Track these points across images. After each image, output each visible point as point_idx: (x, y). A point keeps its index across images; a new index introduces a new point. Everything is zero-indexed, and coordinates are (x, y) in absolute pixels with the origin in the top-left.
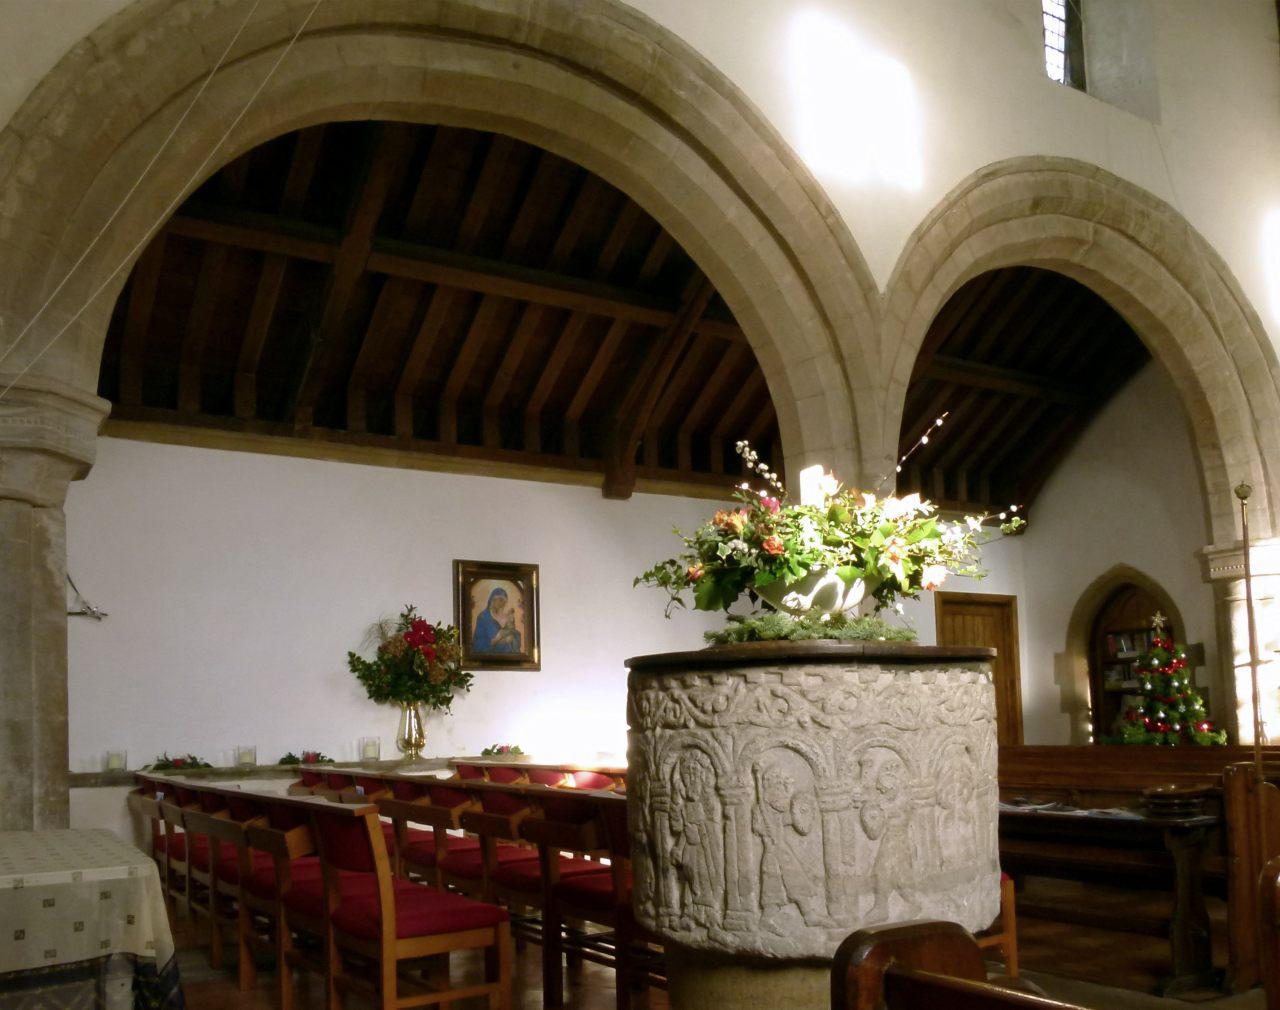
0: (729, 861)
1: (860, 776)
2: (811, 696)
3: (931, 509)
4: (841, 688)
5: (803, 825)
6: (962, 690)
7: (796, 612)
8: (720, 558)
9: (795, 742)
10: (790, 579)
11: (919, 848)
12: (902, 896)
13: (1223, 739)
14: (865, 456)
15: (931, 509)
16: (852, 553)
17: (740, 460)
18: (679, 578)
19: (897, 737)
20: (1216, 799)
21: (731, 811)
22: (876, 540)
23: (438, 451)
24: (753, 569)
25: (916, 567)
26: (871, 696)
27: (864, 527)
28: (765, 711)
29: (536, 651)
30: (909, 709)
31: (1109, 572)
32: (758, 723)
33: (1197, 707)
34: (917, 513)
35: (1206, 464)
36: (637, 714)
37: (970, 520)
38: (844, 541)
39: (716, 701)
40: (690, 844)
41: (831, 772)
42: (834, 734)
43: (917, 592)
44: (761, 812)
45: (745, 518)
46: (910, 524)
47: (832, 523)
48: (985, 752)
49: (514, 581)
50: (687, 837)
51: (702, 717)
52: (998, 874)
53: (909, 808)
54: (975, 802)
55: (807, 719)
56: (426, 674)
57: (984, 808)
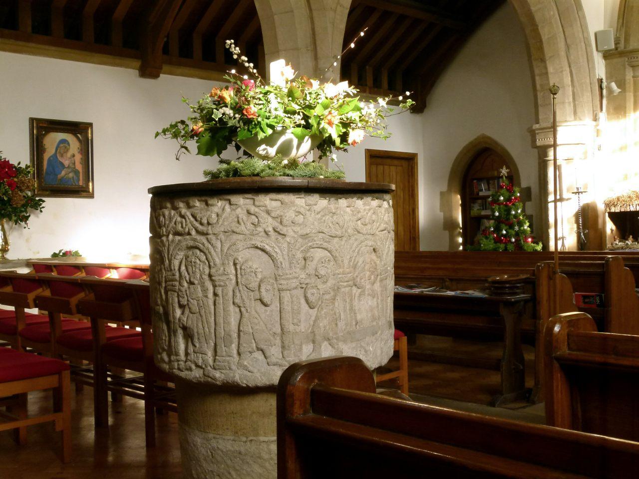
1: (305, 267)
2: (273, 215)
3: (355, 91)
4: (293, 208)
5: (266, 300)
6: (372, 211)
7: (266, 157)
8: (215, 120)
10: (261, 135)
11: (342, 314)
12: (330, 344)
13: (539, 247)
14: (320, 54)
15: (355, 91)
16: (302, 119)
17: (229, 54)
18: (186, 133)
19: (329, 242)
20: (531, 284)
21: (219, 291)
22: (318, 111)
23: (17, 38)
24: (237, 128)
25: (344, 130)
26: (313, 214)
27: (311, 102)
28: (242, 224)
29: (91, 184)
31: (475, 139)
32: (238, 231)
33: (526, 228)
34: (346, 94)
35: (537, 71)
36: (156, 227)
37: (380, 100)
38: (298, 111)
39: (210, 216)
40: (192, 313)
41: (286, 265)
42: (288, 239)
43: (346, 147)
44: (239, 291)
45: (232, 93)
46: (341, 101)
47: (290, 99)
48: (386, 251)
49: (75, 134)
50: (190, 308)
51: (200, 228)
52: (393, 330)
54: (378, 284)
55: (271, 229)
56: (10, 200)
57: (384, 288)
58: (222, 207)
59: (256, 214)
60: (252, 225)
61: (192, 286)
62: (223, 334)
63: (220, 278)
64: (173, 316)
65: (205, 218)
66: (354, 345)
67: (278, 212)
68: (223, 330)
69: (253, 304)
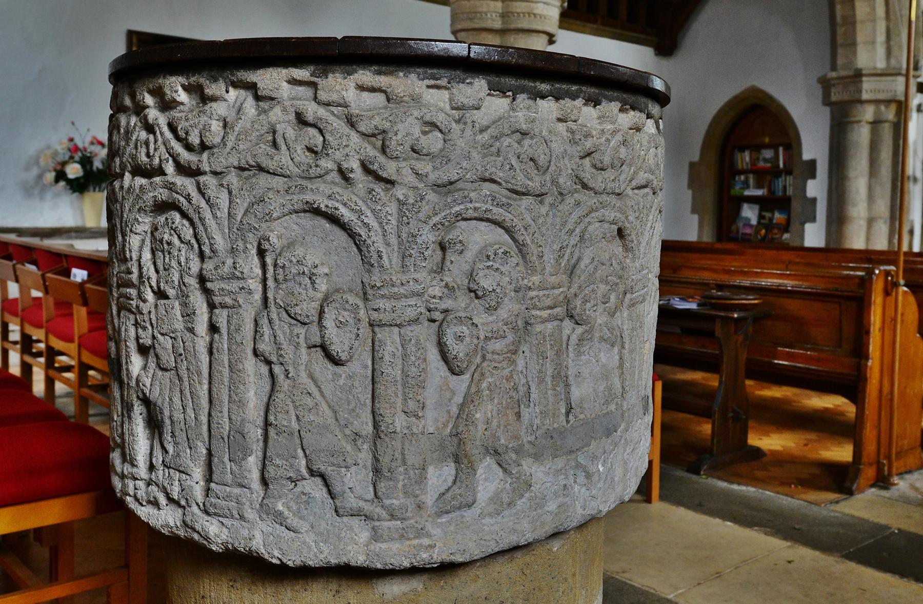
0: (215, 402)
1: (441, 268)
5: (338, 348)
6: (619, 137)
9: (331, 203)
11: (533, 389)
19: (509, 205)
21: (222, 318)
26: (468, 132)
28: (283, 147)
30: (531, 159)
31: (742, 93)
39: (206, 128)
41: (390, 259)
42: (399, 192)
50: (157, 356)
51: (185, 156)
53: (520, 323)
55: (355, 165)
58: (238, 104)
59: (319, 125)
60: (307, 154)
61: (162, 302)
62: (227, 428)
63: (222, 285)
64: (127, 369)
65: (197, 132)
66: (560, 463)
67: (377, 121)
68: (227, 420)
69: (305, 357)
